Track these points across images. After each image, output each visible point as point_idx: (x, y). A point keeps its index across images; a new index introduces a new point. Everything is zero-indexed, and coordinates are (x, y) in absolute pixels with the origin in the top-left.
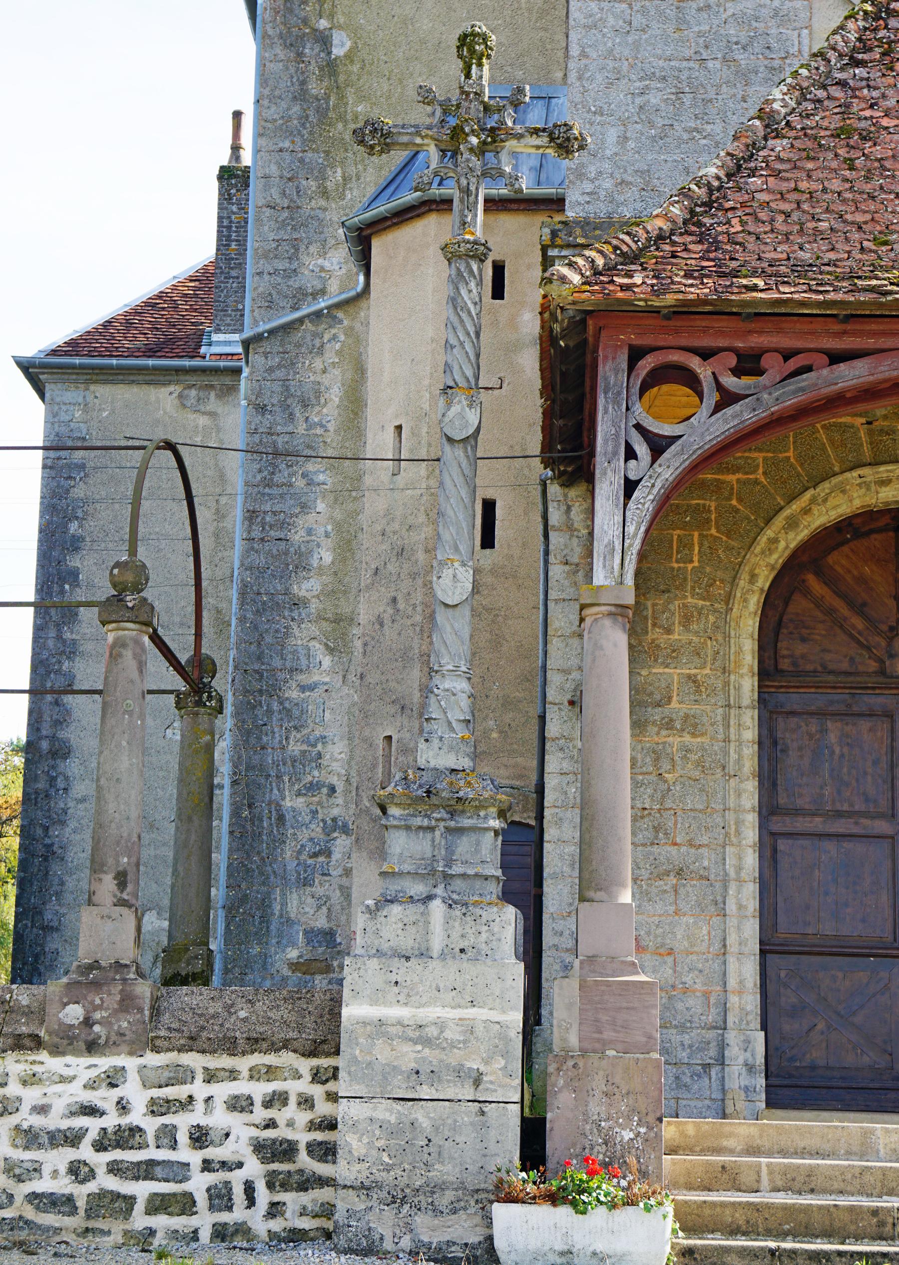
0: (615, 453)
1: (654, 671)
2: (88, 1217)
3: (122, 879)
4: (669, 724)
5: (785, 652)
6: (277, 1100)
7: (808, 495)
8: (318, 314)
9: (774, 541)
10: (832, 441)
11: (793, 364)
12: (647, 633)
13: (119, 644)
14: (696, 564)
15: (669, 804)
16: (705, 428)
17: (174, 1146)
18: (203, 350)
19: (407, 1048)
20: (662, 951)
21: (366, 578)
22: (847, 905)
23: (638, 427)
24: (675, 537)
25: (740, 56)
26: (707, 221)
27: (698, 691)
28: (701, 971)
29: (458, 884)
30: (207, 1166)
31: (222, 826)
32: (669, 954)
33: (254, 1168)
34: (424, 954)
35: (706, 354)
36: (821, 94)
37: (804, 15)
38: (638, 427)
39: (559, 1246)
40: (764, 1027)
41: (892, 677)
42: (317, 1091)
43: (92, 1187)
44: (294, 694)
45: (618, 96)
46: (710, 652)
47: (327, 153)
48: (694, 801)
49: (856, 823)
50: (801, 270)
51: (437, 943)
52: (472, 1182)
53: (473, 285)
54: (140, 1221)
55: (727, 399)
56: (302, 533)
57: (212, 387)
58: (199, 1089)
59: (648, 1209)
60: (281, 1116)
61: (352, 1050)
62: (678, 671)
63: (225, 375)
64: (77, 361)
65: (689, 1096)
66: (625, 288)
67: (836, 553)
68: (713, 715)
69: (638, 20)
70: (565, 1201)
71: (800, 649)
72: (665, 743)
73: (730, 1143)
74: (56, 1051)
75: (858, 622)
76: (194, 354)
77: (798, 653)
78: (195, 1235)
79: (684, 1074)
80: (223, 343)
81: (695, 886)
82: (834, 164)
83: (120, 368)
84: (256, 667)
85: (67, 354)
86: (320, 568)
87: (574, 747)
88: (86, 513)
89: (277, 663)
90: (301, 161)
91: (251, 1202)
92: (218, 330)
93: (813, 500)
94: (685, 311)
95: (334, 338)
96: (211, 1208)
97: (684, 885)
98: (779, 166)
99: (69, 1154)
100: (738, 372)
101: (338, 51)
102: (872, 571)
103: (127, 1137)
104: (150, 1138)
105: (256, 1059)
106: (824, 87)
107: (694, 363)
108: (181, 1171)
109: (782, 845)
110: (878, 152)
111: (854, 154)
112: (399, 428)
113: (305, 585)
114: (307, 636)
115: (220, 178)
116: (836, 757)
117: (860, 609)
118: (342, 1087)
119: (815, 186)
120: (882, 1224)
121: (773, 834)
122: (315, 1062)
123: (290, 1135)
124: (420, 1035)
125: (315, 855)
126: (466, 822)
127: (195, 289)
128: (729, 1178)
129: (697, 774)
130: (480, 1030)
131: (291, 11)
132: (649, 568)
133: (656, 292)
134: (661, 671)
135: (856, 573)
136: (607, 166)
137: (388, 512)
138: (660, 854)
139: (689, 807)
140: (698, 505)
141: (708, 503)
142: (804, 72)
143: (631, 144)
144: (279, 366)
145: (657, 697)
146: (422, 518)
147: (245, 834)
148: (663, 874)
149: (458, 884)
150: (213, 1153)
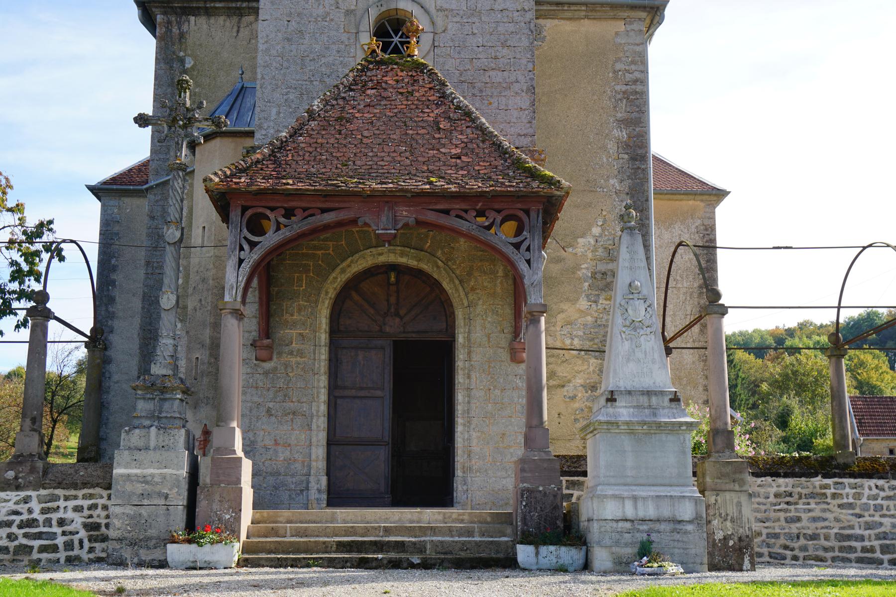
0: (235, 248)
2: (14, 555)
4: (291, 353)
6: (93, 507)
7: (350, 259)
9: (336, 278)
11: (306, 213)
15: (290, 385)
16: (270, 239)
17: (51, 526)
19: (139, 485)
23: (245, 238)
25: (327, 80)
26: (278, 155)
29: (164, 420)
30: (64, 533)
33: (83, 534)
34: (147, 448)
35: (272, 209)
36: (334, 102)
38: (245, 238)
39: (192, 559)
40: (328, 474)
43: (16, 543)
45: (277, 95)
50: (309, 176)
51: (152, 444)
52: (163, 536)
53: (180, 181)
54: (35, 556)
58: (62, 503)
59: (226, 544)
60: (95, 513)
66: (236, 183)
69: (285, 64)
70: (194, 542)
75: (372, 311)
78: (58, 561)
82: (333, 132)
83: (134, 190)
85: (110, 184)
91: (81, 547)
93: (352, 262)
94: (262, 193)
96: (66, 550)
100: (284, 216)
101: (188, 66)
103: (32, 523)
104: (41, 523)
105: (85, 491)
106: (336, 99)
107: (268, 212)
108: (53, 536)
109: (339, 401)
110: (352, 127)
119: (325, 141)
120: (327, 547)
121: (336, 397)
123: (98, 520)
124: (144, 480)
126: (168, 396)
128: (275, 532)
130: (168, 477)
133: (248, 185)
136: (272, 124)
137: (199, 263)
142: (328, 93)
143: (282, 115)
146: (212, 266)
149: (164, 420)
150: (67, 528)
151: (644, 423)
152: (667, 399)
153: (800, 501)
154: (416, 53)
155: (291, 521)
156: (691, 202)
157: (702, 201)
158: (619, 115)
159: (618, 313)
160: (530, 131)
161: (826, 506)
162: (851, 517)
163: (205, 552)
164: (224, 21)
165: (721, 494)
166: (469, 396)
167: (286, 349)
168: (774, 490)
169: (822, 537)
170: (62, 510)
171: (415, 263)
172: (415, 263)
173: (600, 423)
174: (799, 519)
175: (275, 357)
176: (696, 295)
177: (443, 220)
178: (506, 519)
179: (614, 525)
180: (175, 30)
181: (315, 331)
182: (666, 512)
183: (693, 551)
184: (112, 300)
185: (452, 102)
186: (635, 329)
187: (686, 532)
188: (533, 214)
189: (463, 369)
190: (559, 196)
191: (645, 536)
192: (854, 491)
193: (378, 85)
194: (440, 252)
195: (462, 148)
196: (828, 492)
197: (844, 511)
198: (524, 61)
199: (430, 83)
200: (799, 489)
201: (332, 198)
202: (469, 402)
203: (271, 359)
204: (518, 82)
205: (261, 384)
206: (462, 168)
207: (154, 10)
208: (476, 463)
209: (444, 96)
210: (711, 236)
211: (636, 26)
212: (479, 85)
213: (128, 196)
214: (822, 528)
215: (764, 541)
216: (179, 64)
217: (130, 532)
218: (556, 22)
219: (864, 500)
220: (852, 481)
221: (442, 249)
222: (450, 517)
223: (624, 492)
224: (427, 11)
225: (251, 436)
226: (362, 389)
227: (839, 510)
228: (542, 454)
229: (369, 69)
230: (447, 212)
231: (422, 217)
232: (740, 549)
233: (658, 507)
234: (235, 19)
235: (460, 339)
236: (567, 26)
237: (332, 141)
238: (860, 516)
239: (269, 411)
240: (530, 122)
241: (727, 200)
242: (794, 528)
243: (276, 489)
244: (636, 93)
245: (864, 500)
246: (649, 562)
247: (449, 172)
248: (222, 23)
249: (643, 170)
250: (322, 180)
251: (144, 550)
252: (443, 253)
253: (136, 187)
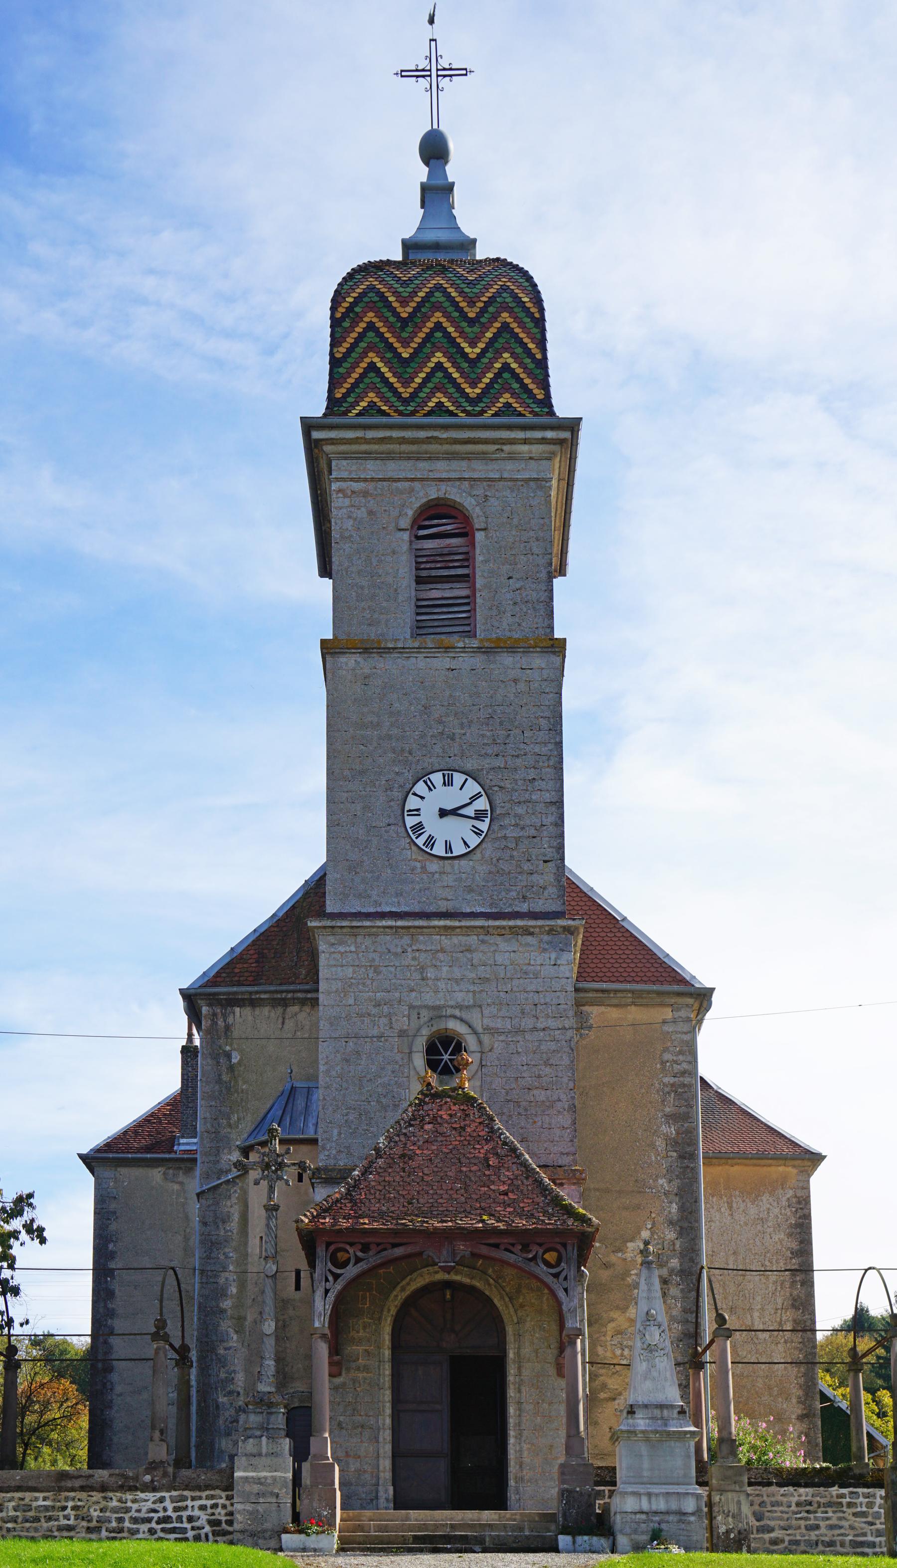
3: (162, 1432)
4: (358, 1369)
7: (409, 1278)
8: (228, 1181)
9: (396, 1296)
11: (380, 1247)
13: (158, 1349)
16: (351, 1271)
17: (182, 1522)
18: (175, 1148)
21: (249, 1302)
27: (369, 1355)
30: (193, 1528)
31: (194, 1408)
33: (208, 1529)
34: (260, 1455)
36: (397, 1139)
37: (407, 1084)
38: (330, 1270)
42: (228, 1503)
44: (222, 1352)
47: (231, 1107)
50: (382, 1215)
51: (264, 1451)
55: (358, 1260)
56: (223, 1280)
57: (181, 1168)
58: (189, 1503)
61: (238, 1487)
63: (188, 1162)
64: (111, 1155)
66: (323, 1224)
73: (364, 1518)
74: (142, 1491)
76: (171, 1151)
80: (186, 1144)
83: (133, 1159)
84: (206, 1340)
85: (105, 1151)
86: (232, 1295)
88: (117, 1238)
89: (214, 1338)
90: (220, 1111)
92: (183, 1137)
93: (411, 1280)
95: (235, 1191)
98: (380, 1171)
99: (148, 1526)
100: (361, 1251)
101: (234, 1061)
103: (167, 1520)
105: (208, 1493)
106: (398, 1136)
107: (348, 1247)
111: (406, 1165)
112: (261, 1238)
113: (226, 1303)
114: (226, 1325)
115: (182, 1052)
118: (235, 1500)
120: (405, 1540)
122: (227, 1493)
123: (219, 1518)
124: (259, 1481)
125: (232, 1422)
126: (274, 1410)
127: (170, 1110)
128: (361, 1528)
129: (368, 1388)
130: (278, 1480)
131: (214, 1042)
133: (333, 1226)
143: (343, 1136)
144: (213, 1204)
147: (202, 1412)
149: (271, 1431)
151: (656, 1432)
152: (676, 1411)
153: (819, 1510)
154: (467, 1086)
155: (373, 1519)
156: (781, 1169)
157: (794, 1166)
158: (667, 1110)
159: (638, 1337)
160: (572, 1149)
161: (841, 1515)
162: (863, 1525)
163: (312, 1541)
164: (269, 1012)
165: (724, 1494)
166: (520, 1410)
167: (353, 1365)
168: (794, 1499)
169: (838, 1544)
170: (190, 1509)
171: (468, 1281)
172: (468, 1281)
173: (622, 1431)
174: (817, 1527)
175: (344, 1372)
176: (787, 1285)
177: (495, 1253)
178: (552, 1518)
179: (633, 1516)
180: (221, 1023)
181: (379, 1348)
182: (674, 1506)
183: (695, 1538)
184: (111, 1294)
185: (499, 1137)
186: (651, 1351)
187: (689, 1523)
188: (569, 1248)
189: (514, 1384)
190: (590, 1232)
191: (656, 1525)
192: (867, 1500)
193: (434, 1120)
194: (490, 1270)
195: (509, 1185)
196: (844, 1501)
197: (857, 1519)
198: (565, 1080)
199: (479, 1117)
200: (818, 1499)
201: (400, 1236)
202: (520, 1416)
203: (340, 1374)
204: (560, 1100)
206: (509, 1205)
207: (199, 1002)
208: (527, 1474)
209: (492, 1131)
210: (806, 1211)
211: (683, 1013)
212: (523, 1104)
213: (126, 1166)
214: (839, 1535)
215: (786, 1548)
216: (226, 1059)
217: (250, 1525)
218: (603, 1009)
219: (876, 1509)
220: (866, 1490)
222: (504, 1517)
223: (641, 1489)
224: (475, 1032)
227: (854, 1519)
228: (579, 1460)
229: (426, 1103)
230: (496, 1246)
231: (476, 1251)
232: (740, 1541)
233: (667, 1502)
234: (280, 1010)
235: (511, 1355)
236: (614, 1014)
237: (398, 1179)
238: (872, 1524)
240: (572, 1141)
241: (824, 1164)
242: (813, 1536)
244: (684, 1085)
245: (876, 1509)
246: (658, 1544)
247: (498, 1209)
248: (267, 1014)
249: (692, 1169)
250: (393, 1219)
251: (266, 1538)
252: (494, 1271)
253: (134, 1156)
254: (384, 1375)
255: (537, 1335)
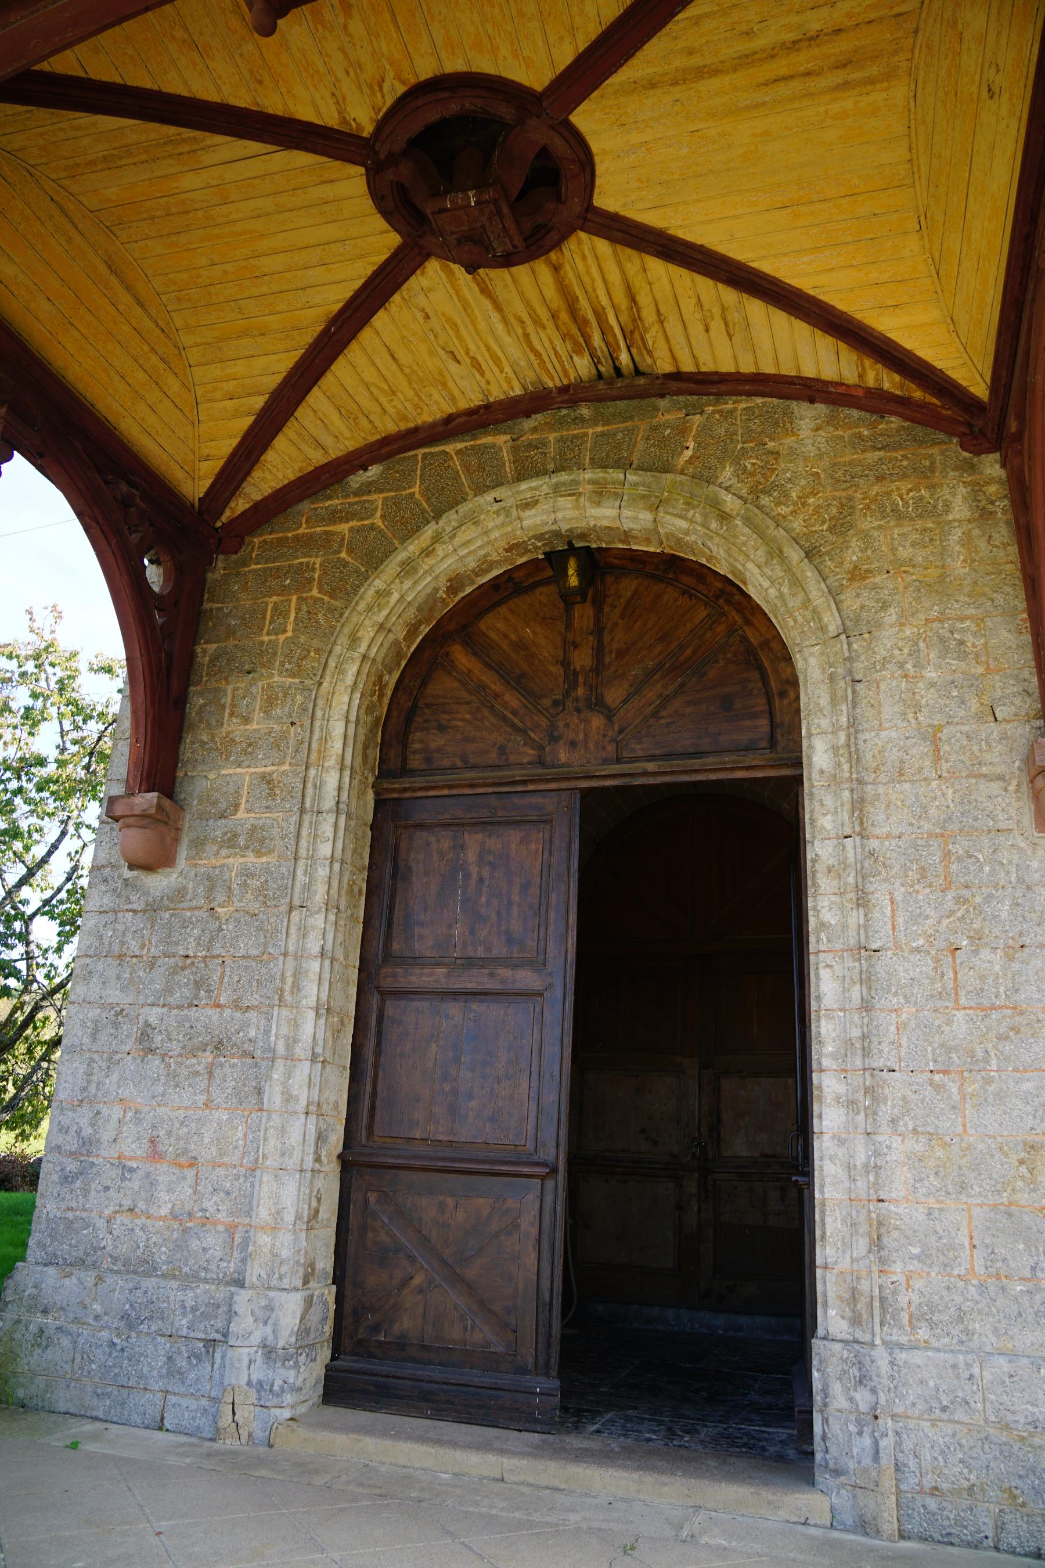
1: (223, 772)
4: (230, 841)
5: (417, 746)
10: (467, 467)
12: (222, 724)
14: (290, 634)
20: (182, 1160)
22: (470, 1096)
24: (270, 606)
28: (228, 1193)
32: (191, 1165)
41: (553, 767)
46: (292, 742)
48: (249, 945)
49: (492, 975)
62: (252, 770)
65: (182, 1389)
67: (491, 615)
68: (285, 825)
71: (437, 741)
72: (223, 866)
75: (512, 699)
77: (433, 745)
79: (180, 1353)
81: (234, 1065)
87: (119, 877)
93: (437, 538)
97: (222, 1065)
102: (534, 632)
116: (473, 882)
117: (517, 681)
129: (255, 906)
132: (236, 646)
134: (231, 771)
135: (514, 637)
138: (197, 1020)
139: (242, 952)
140: (301, 564)
141: (312, 560)
145: (223, 806)
148: (198, 1049)
166: (867, 979)
167: (218, 829)
202: (866, 1007)
205: (133, 946)
208: (911, 1280)
221: (736, 462)
225: (84, 1122)
226: (470, 963)
235: (819, 755)
239: (145, 1035)
243: (131, 1327)
254: (312, 858)
255: (931, 674)
